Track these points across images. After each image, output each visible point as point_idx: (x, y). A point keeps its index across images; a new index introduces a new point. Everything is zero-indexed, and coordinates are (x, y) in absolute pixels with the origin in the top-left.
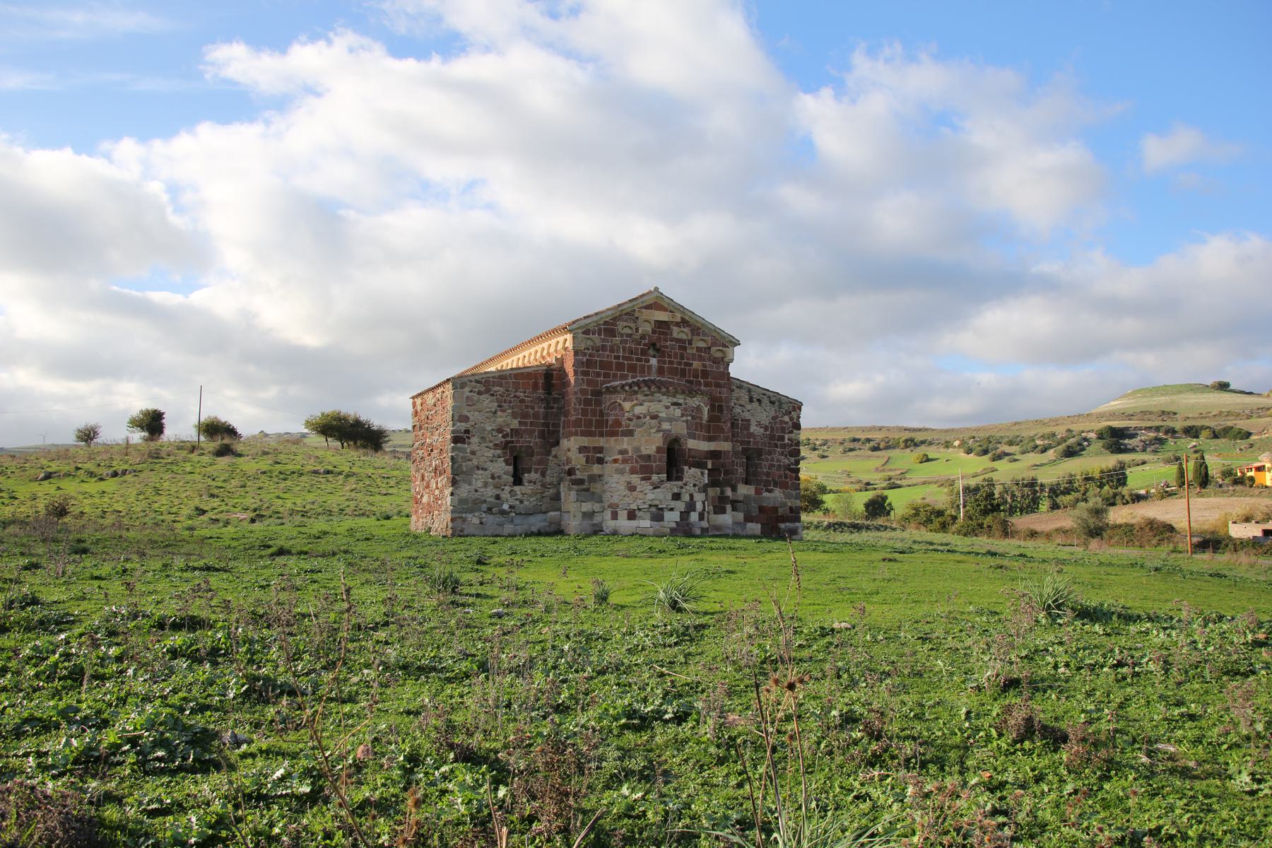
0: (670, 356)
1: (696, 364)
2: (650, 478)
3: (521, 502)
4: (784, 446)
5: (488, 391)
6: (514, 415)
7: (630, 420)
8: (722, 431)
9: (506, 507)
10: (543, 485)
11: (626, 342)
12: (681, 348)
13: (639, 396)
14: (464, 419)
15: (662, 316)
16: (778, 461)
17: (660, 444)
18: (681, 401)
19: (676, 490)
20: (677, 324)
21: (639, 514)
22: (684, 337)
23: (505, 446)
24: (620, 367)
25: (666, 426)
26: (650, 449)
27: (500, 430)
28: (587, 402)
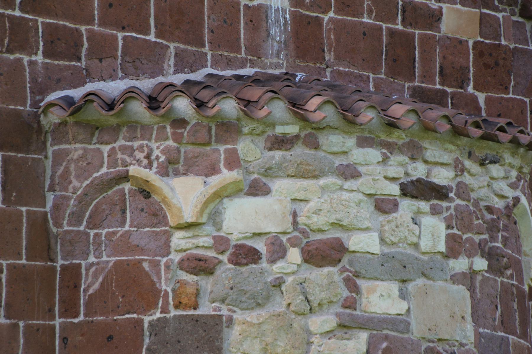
7: (200, 266)
13: (249, 148)
18: (443, 177)
25: (382, 299)
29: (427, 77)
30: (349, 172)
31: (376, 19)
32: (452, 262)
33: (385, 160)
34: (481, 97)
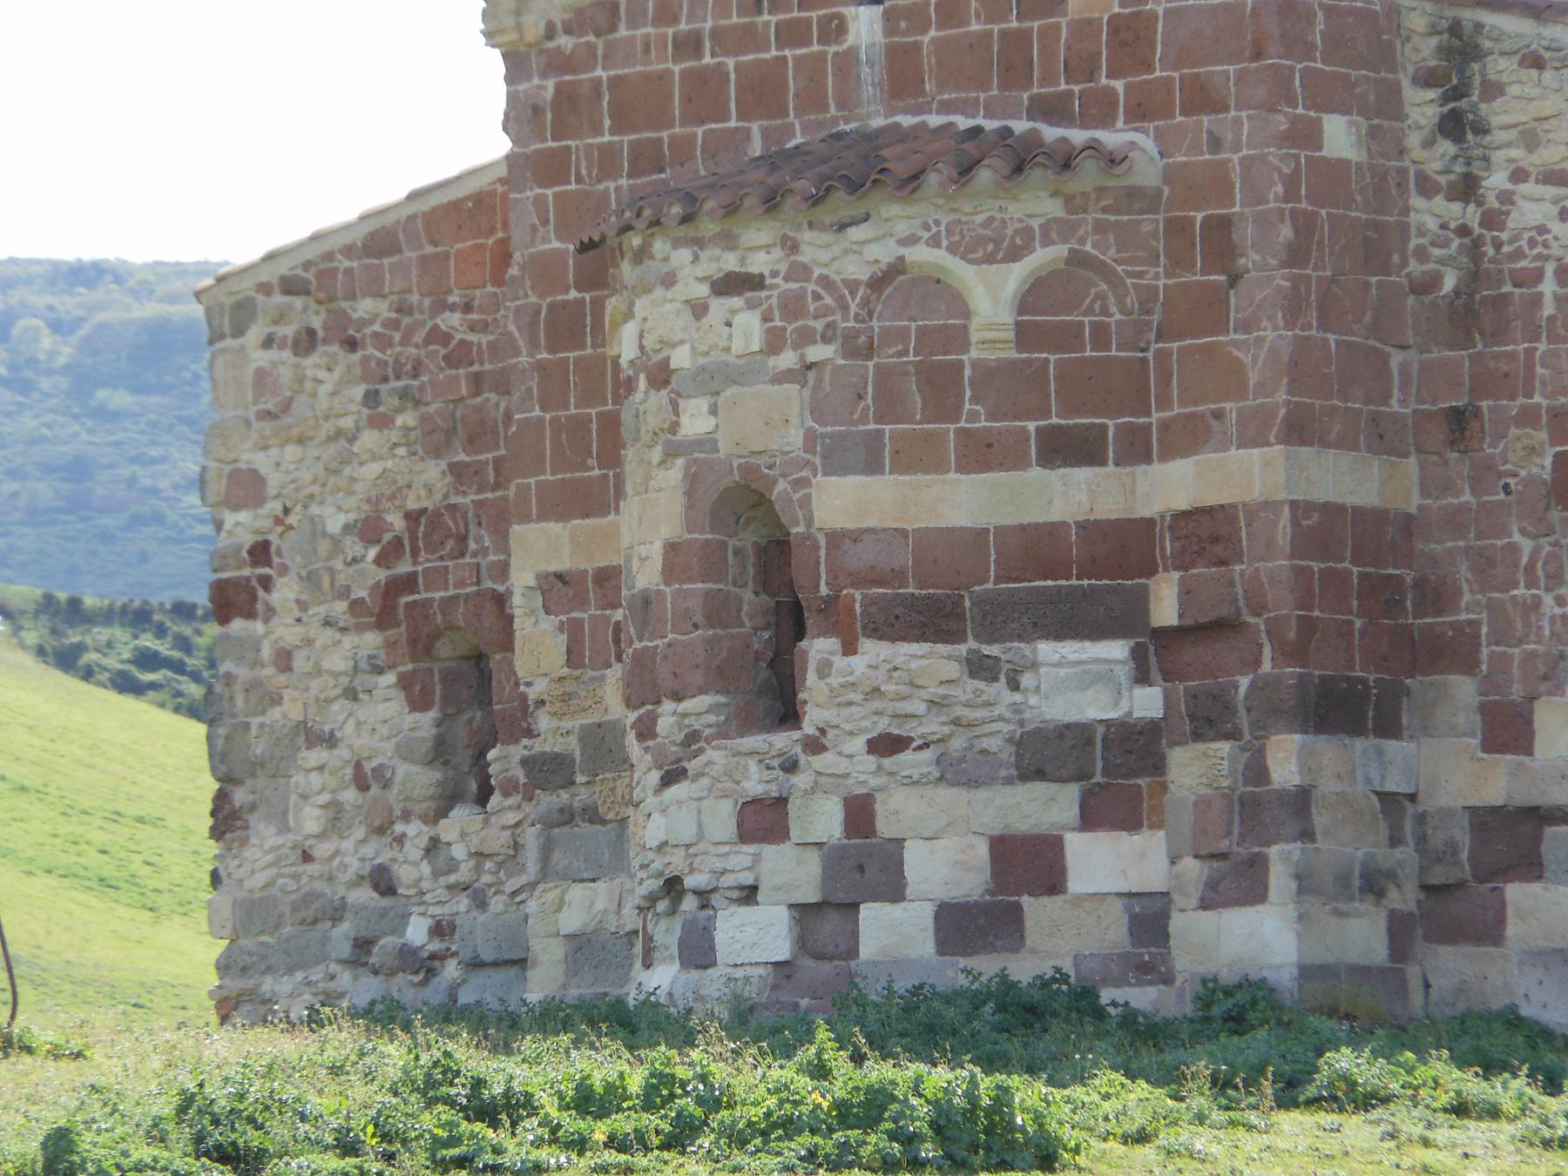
3: (481, 903)
14: (245, 488)
18: (759, 263)
19: (755, 783)
23: (384, 608)
27: (369, 529)
30: (669, 280)
31: (986, 23)
32: (773, 361)
33: (696, 259)
34: (1119, 85)
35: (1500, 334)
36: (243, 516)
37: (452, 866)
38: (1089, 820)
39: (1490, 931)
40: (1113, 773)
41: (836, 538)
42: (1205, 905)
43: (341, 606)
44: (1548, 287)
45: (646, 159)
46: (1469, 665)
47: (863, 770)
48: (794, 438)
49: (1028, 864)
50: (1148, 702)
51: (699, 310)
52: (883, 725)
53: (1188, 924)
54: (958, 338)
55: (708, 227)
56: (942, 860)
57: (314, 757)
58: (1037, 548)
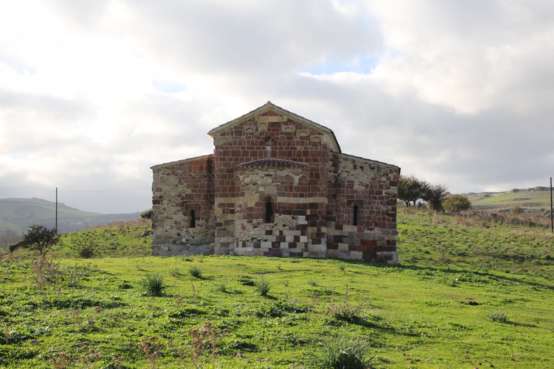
0: (280, 144)
1: (299, 148)
2: (251, 222)
3: (193, 237)
4: (382, 198)
5: (173, 173)
6: (189, 187)
7: (243, 186)
8: (319, 190)
9: (184, 240)
10: (207, 227)
11: (250, 138)
12: (288, 138)
13: (247, 172)
15: (274, 119)
16: (377, 208)
17: (257, 200)
18: (271, 173)
19: (268, 229)
20: (286, 123)
21: (247, 243)
22: (289, 131)
23: (182, 205)
24: (245, 154)
25: (261, 189)
26: (252, 204)
27: (179, 196)
28: (224, 177)
29: (294, 156)
30: (258, 174)
35: (340, 187)
36: (158, 193)
37: (190, 233)
38: (302, 235)
39: (336, 247)
40: (303, 229)
41: (279, 203)
42: (313, 244)
43: (174, 204)
44: (346, 183)
45: (236, 160)
46: (334, 221)
47: (282, 228)
48: (275, 192)
49: (297, 239)
50: (306, 223)
51: (262, 178)
52: (284, 223)
53: (310, 246)
54: (293, 183)
55: (265, 169)
56: (289, 238)
57: (169, 220)
58: (299, 206)
